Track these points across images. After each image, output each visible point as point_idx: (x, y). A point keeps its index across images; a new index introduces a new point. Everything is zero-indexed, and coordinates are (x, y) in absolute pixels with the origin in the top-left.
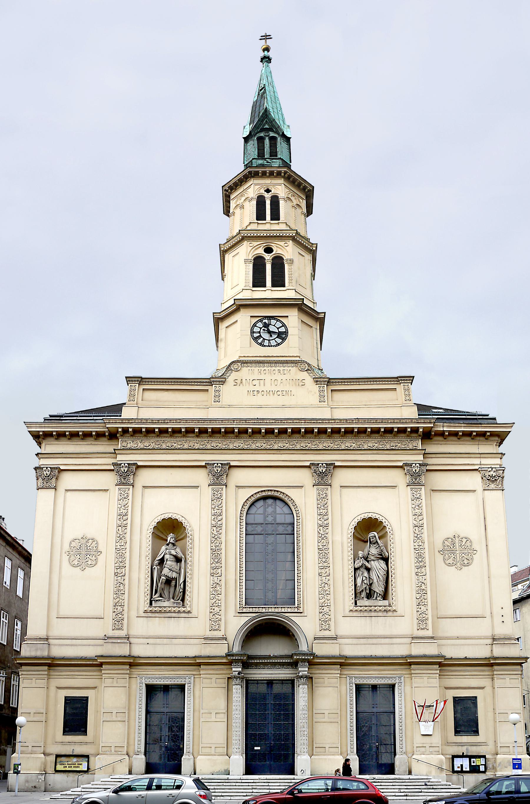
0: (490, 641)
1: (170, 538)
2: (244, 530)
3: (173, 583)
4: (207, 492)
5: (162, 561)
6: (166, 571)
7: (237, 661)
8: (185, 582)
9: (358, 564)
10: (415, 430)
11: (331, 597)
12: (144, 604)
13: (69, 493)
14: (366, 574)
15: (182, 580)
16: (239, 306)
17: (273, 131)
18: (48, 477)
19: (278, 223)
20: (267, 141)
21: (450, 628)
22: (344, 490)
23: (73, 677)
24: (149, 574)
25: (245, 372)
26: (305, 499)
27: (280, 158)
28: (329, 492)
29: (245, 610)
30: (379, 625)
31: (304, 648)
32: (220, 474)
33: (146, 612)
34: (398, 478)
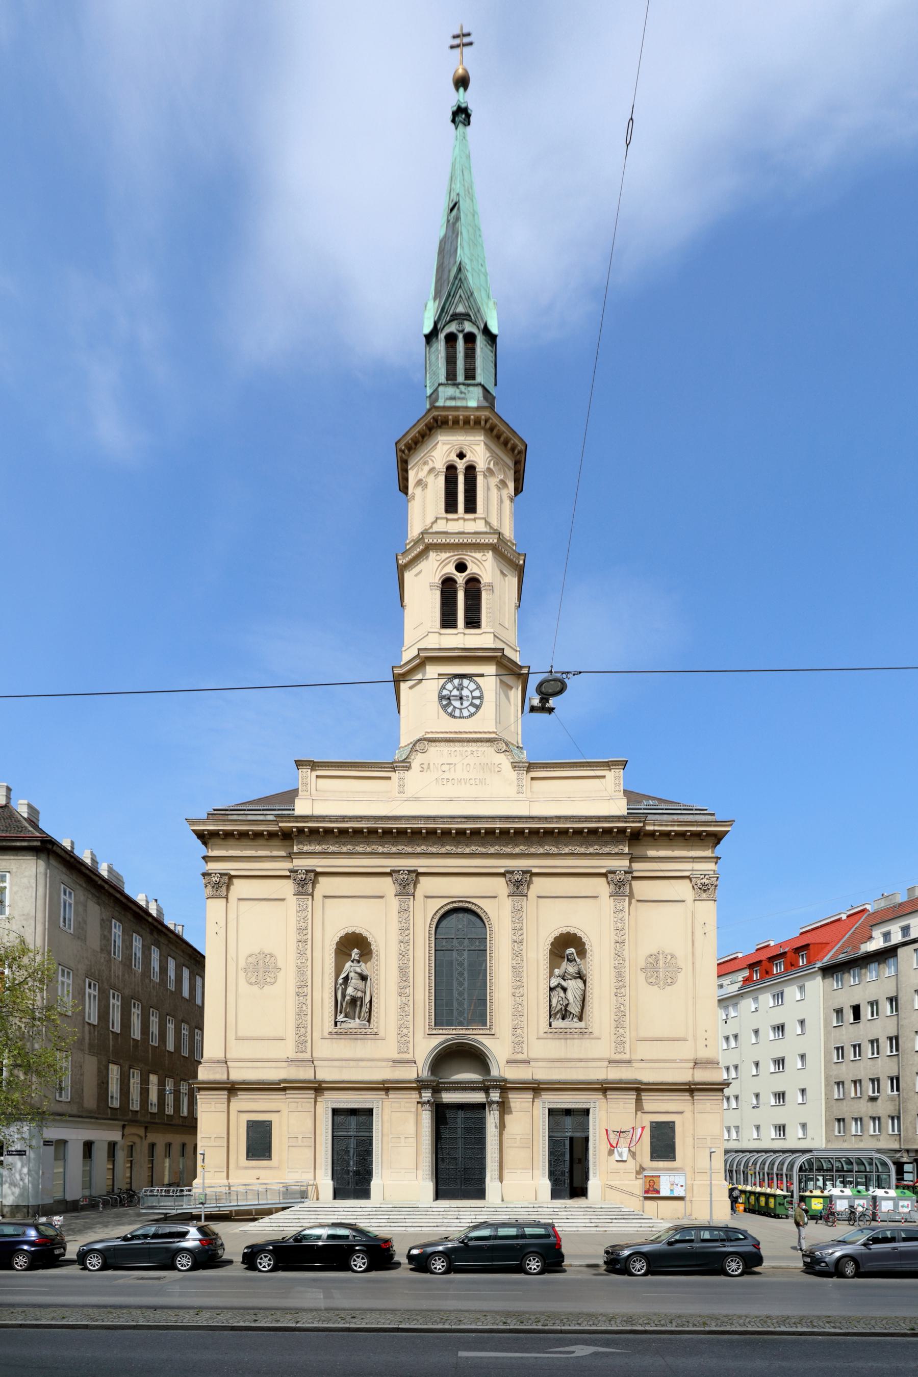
0: (692, 1065)
1: (355, 953)
2: (433, 945)
3: (359, 1003)
4: (394, 903)
5: (346, 979)
6: (350, 991)
7: (426, 1087)
8: (371, 1001)
9: (554, 982)
10: (622, 831)
11: (524, 1018)
12: (329, 1026)
13: (241, 903)
14: (562, 994)
15: (367, 999)
16: (424, 660)
17: (470, 321)
18: (221, 885)
19: (475, 520)
20: (460, 344)
21: (644, 1051)
22: (541, 900)
23: (254, 1100)
24: (333, 993)
25: (436, 753)
26: (498, 909)
27: (480, 384)
28: (524, 903)
29: (434, 1032)
30: (576, 1048)
31: (494, 1072)
32: (407, 883)
33: (330, 1033)
34: (601, 886)
